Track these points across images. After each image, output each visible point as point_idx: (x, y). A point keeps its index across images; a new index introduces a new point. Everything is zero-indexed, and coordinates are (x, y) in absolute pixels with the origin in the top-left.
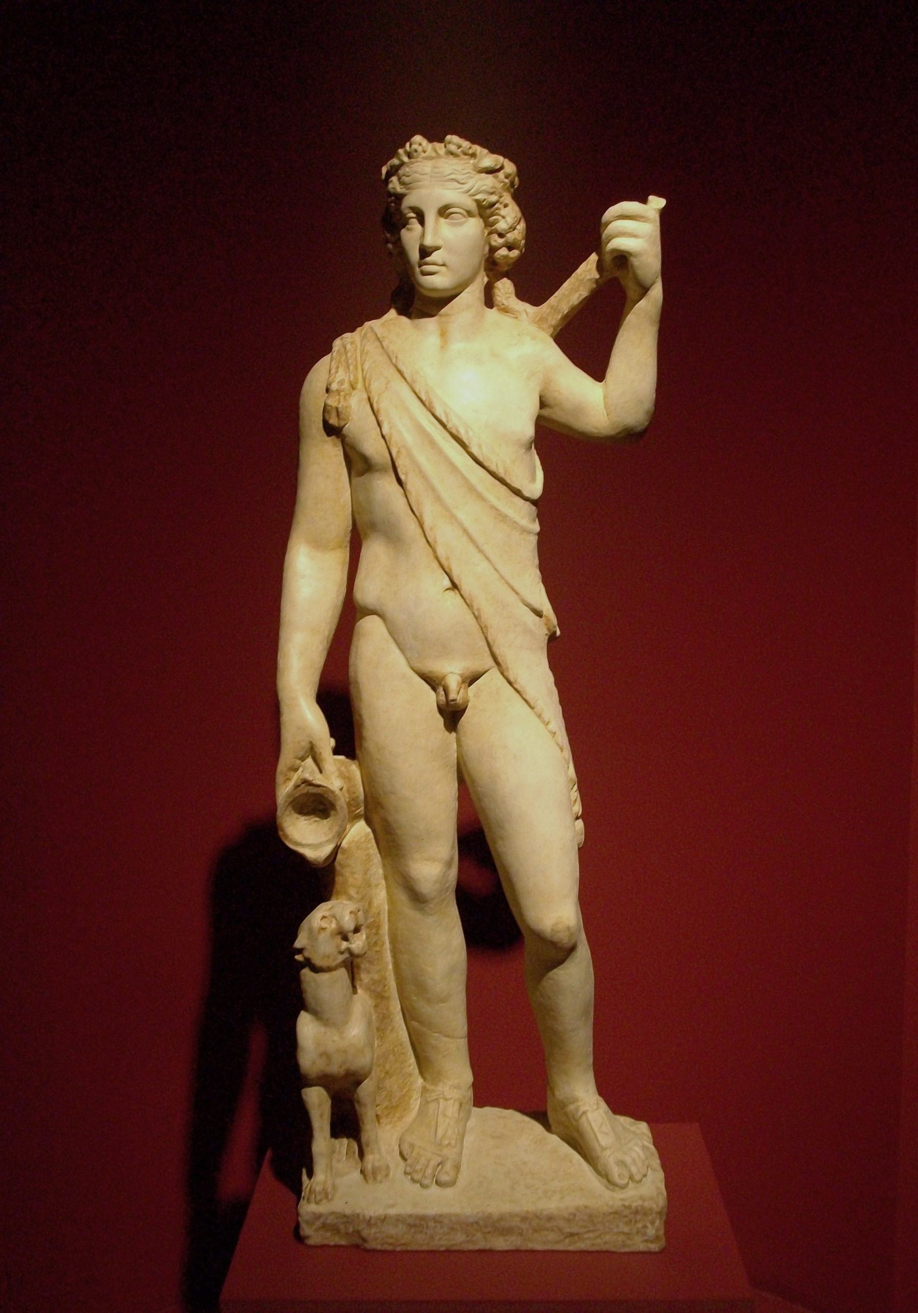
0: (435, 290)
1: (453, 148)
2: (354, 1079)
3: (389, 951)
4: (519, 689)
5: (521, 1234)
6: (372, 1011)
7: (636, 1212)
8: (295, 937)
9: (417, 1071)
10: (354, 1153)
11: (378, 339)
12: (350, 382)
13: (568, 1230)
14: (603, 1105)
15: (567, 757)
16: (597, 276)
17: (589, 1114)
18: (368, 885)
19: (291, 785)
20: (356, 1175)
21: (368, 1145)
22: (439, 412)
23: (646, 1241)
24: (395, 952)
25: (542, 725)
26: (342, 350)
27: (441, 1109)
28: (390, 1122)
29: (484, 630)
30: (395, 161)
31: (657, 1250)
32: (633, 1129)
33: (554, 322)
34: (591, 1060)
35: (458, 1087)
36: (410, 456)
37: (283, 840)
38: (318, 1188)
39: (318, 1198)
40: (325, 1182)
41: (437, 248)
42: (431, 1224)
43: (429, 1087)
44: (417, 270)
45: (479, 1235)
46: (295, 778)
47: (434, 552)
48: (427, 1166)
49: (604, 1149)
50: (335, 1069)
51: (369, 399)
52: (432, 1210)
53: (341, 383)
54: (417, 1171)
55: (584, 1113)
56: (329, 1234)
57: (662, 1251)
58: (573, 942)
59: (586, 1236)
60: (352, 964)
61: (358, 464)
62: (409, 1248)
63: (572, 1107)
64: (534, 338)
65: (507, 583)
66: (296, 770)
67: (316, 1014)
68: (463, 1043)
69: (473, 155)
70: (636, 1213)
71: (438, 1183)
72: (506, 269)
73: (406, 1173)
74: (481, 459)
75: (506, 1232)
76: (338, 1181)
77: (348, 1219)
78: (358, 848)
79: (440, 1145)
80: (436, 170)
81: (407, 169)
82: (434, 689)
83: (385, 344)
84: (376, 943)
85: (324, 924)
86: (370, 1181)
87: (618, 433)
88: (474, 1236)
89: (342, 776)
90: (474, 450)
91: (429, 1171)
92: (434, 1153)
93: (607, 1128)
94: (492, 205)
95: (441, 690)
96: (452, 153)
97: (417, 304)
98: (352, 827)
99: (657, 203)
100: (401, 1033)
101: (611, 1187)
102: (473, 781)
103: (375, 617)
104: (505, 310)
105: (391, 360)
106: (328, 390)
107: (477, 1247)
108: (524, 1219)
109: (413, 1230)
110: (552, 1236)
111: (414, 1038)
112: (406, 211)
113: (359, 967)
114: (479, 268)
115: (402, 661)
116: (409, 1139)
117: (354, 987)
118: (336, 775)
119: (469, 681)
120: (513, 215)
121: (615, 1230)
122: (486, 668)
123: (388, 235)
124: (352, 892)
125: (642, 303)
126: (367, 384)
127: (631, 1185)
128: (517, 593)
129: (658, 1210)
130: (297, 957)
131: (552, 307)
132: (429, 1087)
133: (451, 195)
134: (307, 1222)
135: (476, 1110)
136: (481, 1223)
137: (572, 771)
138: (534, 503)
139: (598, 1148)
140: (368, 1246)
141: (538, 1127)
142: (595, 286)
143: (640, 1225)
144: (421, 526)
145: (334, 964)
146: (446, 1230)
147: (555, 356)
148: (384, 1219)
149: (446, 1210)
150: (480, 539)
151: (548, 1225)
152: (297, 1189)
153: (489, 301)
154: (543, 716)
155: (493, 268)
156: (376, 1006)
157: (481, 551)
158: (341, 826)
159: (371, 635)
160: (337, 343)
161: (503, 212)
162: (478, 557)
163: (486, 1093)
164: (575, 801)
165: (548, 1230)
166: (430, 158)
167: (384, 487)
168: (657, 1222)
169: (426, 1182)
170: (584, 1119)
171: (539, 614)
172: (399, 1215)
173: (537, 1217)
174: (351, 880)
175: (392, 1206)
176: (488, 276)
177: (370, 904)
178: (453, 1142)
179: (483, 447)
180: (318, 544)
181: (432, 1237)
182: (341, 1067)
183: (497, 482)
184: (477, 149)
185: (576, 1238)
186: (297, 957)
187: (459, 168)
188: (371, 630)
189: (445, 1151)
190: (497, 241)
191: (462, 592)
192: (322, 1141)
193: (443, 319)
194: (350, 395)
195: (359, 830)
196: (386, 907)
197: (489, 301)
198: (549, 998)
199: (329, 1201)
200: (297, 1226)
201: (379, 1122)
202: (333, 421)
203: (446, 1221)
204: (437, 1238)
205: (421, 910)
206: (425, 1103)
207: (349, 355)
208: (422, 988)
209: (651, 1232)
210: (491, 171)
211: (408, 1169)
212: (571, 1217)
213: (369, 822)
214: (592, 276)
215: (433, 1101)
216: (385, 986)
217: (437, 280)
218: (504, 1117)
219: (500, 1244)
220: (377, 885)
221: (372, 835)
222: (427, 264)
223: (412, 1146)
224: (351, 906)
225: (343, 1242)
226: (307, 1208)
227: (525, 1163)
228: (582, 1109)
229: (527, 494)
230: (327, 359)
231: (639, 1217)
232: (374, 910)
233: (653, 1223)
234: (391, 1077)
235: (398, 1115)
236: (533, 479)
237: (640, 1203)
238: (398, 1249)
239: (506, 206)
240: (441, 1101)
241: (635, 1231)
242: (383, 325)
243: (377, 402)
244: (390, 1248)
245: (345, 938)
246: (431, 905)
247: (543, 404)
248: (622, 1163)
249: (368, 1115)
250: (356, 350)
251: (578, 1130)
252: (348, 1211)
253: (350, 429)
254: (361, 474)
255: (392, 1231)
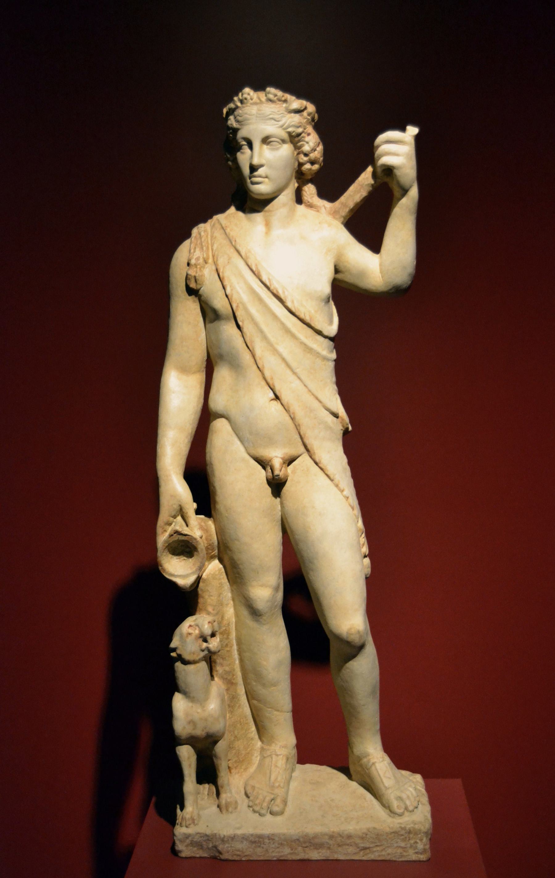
0: (262, 194)
1: (271, 96)
2: (212, 740)
3: (236, 651)
4: (323, 467)
5: (329, 848)
6: (225, 693)
7: (410, 832)
8: (170, 640)
9: (257, 737)
10: (213, 793)
11: (223, 228)
12: (204, 258)
13: (362, 845)
14: (387, 759)
15: (357, 514)
16: (373, 182)
17: (377, 765)
18: (221, 604)
19: (167, 534)
20: (215, 809)
21: (222, 787)
22: (265, 278)
23: (416, 853)
24: (240, 652)
25: (340, 493)
26: (198, 236)
27: (273, 762)
28: (238, 773)
29: (297, 427)
30: (232, 105)
31: (424, 859)
32: (411, 778)
33: (344, 214)
34: (378, 727)
35: (285, 747)
36: (246, 309)
37: (162, 572)
38: (188, 816)
39: (188, 823)
40: (192, 812)
41: (262, 166)
42: (267, 841)
43: (265, 747)
44: (249, 181)
45: (300, 849)
46: (170, 530)
47: (263, 374)
48: (264, 801)
49: (387, 788)
50: (199, 732)
51: (217, 270)
52: (267, 831)
53: (198, 259)
54: (256, 805)
55: (374, 764)
56: (196, 849)
57: (429, 860)
58: (362, 641)
59: (375, 849)
60: (210, 659)
61: (210, 314)
62: (251, 859)
63: (365, 760)
64: (330, 225)
65: (313, 394)
66: (170, 524)
67: (185, 694)
68: (288, 716)
69: (285, 101)
70: (409, 833)
71: (271, 813)
72: (310, 177)
73: (249, 806)
74: (293, 310)
75: (319, 846)
76: (201, 813)
77: (208, 838)
78: (214, 578)
79: (273, 787)
80: (259, 112)
81: (240, 112)
82: (264, 468)
83: (228, 231)
84: (227, 645)
85: (190, 631)
86: (224, 811)
87: (391, 290)
88: (296, 849)
89: (201, 528)
90: (289, 304)
91: (265, 804)
92: (268, 792)
93: (389, 774)
94: (299, 135)
95: (269, 469)
96: (270, 100)
97: (249, 204)
98: (209, 564)
99: (412, 131)
100: (245, 709)
101: (392, 815)
102: (292, 532)
103: (223, 420)
104: (310, 206)
105: (231, 243)
106: (188, 264)
107: (298, 858)
108: (331, 837)
109: (254, 845)
110: (351, 850)
111: (255, 715)
112: (240, 140)
113: (215, 662)
114: (292, 176)
115: (242, 449)
116: (251, 783)
117: (212, 676)
118: (198, 528)
119: (288, 462)
120: (314, 141)
121: (395, 845)
122: (300, 453)
123: (229, 156)
124: (210, 609)
125: (404, 201)
126: (215, 260)
127: (406, 814)
128: (320, 402)
129: (425, 830)
130: (172, 654)
131: (342, 204)
132: (265, 747)
133: (270, 129)
134: (181, 841)
135: (299, 766)
136: (301, 840)
137: (360, 524)
138: (332, 339)
139: (383, 789)
140: (223, 857)
141: (342, 777)
142: (371, 189)
143: (412, 842)
144: (254, 356)
145: (197, 658)
146: (276, 845)
147: (345, 237)
148: (233, 838)
149: (276, 831)
150: (294, 364)
151: (348, 842)
152: (172, 821)
153: (299, 199)
154: (340, 486)
155: (301, 177)
156: (227, 690)
157: (294, 373)
158: (201, 563)
159: (221, 432)
160: (195, 231)
161: (307, 139)
162: (292, 378)
163: (306, 753)
164: (363, 544)
165: (348, 845)
166: (256, 104)
167: (228, 329)
168: (425, 839)
169: (263, 812)
170: (373, 768)
171: (336, 416)
172: (244, 834)
173: (341, 836)
174: (209, 600)
175: (239, 828)
176: (298, 182)
177: (223, 617)
178: (282, 785)
179: (295, 302)
180: (184, 370)
181: (267, 850)
182: (203, 731)
183: (305, 326)
184: (288, 96)
185: (368, 851)
186: (172, 654)
187: (276, 110)
188: (220, 428)
189: (277, 791)
190: (303, 159)
191: (282, 402)
192: (190, 784)
193: (267, 214)
194: (204, 267)
195: (214, 566)
196: (234, 620)
197: (299, 199)
198: (347, 682)
199: (195, 825)
200: (174, 844)
201: (230, 772)
202: (193, 285)
203: (277, 839)
204: (271, 851)
205: (257, 621)
206: (263, 758)
207: (203, 240)
208: (259, 676)
209: (420, 846)
210: (298, 111)
211: (251, 804)
212: (364, 835)
213: (221, 561)
214: (369, 182)
215: (268, 756)
216: (233, 675)
217: (262, 187)
218: (320, 770)
219: (315, 855)
220: (227, 605)
221: (223, 570)
222: (255, 177)
223: (253, 787)
224: (210, 618)
225: (205, 855)
226: (180, 831)
227: (332, 800)
228: (372, 761)
229: (326, 333)
230: (187, 243)
231: (411, 836)
232: (225, 622)
233: (421, 840)
234: (238, 740)
235: (243, 767)
236: (331, 322)
237: (412, 825)
238: (244, 859)
239: (309, 134)
240: (274, 756)
241: (409, 845)
242: (226, 218)
243: (223, 272)
244: (237, 858)
245: (205, 641)
246: (264, 618)
247: (337, 270)
248: (400, 799)
249: (222, 765)
250: (207, 236)
251: (369, 776)
252: (208, 832)
253: (205, 290)
254: (212, 321)
255: (239, 846)
